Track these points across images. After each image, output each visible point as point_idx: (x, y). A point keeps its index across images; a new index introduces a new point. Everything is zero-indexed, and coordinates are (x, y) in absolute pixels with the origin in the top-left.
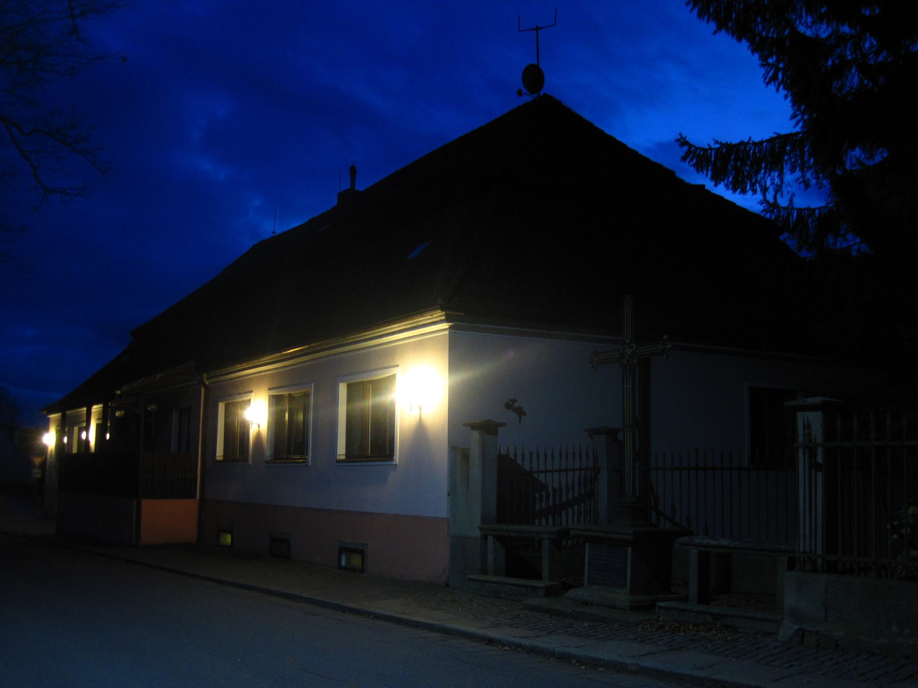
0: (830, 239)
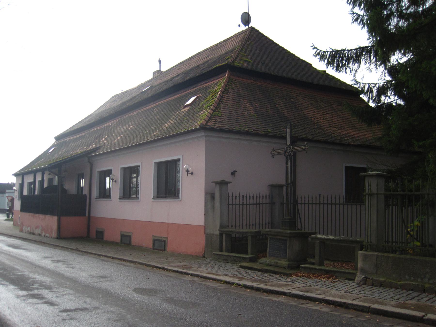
0: (383, 98)
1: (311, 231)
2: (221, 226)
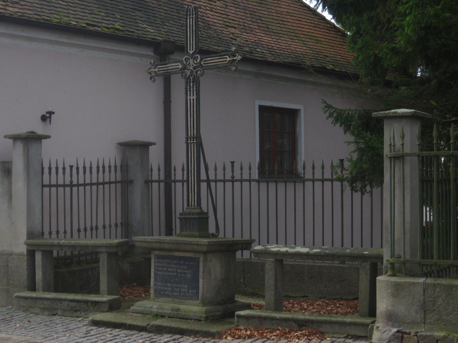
1: (240, 238)
2: (31, 235)
